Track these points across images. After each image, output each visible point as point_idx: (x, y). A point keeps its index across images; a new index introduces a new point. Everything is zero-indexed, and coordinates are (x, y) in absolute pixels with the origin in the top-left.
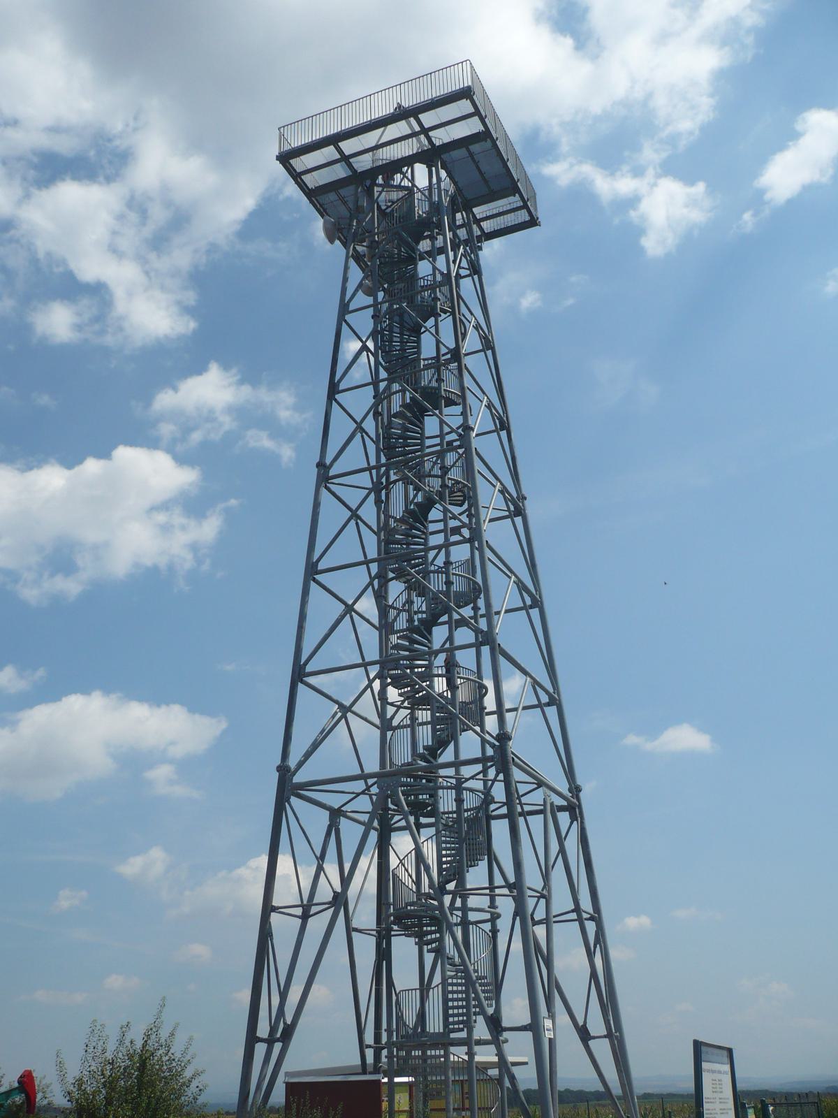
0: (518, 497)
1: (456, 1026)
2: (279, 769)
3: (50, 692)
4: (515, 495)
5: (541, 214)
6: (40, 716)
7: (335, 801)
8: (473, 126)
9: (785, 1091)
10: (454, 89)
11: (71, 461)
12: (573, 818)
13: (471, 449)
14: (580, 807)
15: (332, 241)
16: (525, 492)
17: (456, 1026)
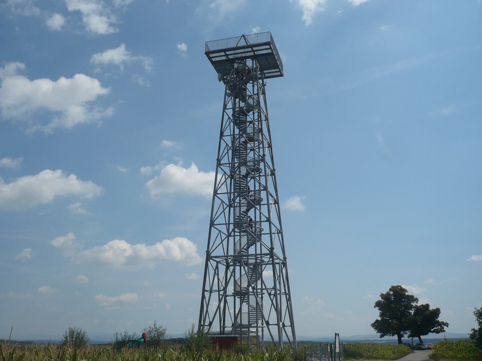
0: (273, 170)
1: (253, 323)
2: (206, 252)
3: (34, 171)
4: (272, 169)
5: (284, 72)
6: (25, 182)
7: (218, 260)
8: (270, 51)
9: (318, 342)
10: (265, 42)
11: (55, 78)
12: (284, 266)
13: (265, 161)
14: (286, 263)
15: (220, 81)
16: (275, 168)
17: (253, 323)
